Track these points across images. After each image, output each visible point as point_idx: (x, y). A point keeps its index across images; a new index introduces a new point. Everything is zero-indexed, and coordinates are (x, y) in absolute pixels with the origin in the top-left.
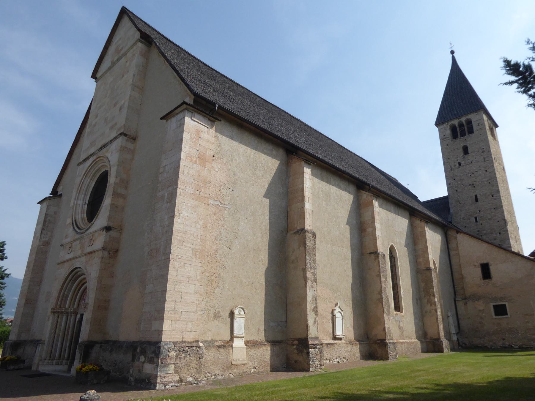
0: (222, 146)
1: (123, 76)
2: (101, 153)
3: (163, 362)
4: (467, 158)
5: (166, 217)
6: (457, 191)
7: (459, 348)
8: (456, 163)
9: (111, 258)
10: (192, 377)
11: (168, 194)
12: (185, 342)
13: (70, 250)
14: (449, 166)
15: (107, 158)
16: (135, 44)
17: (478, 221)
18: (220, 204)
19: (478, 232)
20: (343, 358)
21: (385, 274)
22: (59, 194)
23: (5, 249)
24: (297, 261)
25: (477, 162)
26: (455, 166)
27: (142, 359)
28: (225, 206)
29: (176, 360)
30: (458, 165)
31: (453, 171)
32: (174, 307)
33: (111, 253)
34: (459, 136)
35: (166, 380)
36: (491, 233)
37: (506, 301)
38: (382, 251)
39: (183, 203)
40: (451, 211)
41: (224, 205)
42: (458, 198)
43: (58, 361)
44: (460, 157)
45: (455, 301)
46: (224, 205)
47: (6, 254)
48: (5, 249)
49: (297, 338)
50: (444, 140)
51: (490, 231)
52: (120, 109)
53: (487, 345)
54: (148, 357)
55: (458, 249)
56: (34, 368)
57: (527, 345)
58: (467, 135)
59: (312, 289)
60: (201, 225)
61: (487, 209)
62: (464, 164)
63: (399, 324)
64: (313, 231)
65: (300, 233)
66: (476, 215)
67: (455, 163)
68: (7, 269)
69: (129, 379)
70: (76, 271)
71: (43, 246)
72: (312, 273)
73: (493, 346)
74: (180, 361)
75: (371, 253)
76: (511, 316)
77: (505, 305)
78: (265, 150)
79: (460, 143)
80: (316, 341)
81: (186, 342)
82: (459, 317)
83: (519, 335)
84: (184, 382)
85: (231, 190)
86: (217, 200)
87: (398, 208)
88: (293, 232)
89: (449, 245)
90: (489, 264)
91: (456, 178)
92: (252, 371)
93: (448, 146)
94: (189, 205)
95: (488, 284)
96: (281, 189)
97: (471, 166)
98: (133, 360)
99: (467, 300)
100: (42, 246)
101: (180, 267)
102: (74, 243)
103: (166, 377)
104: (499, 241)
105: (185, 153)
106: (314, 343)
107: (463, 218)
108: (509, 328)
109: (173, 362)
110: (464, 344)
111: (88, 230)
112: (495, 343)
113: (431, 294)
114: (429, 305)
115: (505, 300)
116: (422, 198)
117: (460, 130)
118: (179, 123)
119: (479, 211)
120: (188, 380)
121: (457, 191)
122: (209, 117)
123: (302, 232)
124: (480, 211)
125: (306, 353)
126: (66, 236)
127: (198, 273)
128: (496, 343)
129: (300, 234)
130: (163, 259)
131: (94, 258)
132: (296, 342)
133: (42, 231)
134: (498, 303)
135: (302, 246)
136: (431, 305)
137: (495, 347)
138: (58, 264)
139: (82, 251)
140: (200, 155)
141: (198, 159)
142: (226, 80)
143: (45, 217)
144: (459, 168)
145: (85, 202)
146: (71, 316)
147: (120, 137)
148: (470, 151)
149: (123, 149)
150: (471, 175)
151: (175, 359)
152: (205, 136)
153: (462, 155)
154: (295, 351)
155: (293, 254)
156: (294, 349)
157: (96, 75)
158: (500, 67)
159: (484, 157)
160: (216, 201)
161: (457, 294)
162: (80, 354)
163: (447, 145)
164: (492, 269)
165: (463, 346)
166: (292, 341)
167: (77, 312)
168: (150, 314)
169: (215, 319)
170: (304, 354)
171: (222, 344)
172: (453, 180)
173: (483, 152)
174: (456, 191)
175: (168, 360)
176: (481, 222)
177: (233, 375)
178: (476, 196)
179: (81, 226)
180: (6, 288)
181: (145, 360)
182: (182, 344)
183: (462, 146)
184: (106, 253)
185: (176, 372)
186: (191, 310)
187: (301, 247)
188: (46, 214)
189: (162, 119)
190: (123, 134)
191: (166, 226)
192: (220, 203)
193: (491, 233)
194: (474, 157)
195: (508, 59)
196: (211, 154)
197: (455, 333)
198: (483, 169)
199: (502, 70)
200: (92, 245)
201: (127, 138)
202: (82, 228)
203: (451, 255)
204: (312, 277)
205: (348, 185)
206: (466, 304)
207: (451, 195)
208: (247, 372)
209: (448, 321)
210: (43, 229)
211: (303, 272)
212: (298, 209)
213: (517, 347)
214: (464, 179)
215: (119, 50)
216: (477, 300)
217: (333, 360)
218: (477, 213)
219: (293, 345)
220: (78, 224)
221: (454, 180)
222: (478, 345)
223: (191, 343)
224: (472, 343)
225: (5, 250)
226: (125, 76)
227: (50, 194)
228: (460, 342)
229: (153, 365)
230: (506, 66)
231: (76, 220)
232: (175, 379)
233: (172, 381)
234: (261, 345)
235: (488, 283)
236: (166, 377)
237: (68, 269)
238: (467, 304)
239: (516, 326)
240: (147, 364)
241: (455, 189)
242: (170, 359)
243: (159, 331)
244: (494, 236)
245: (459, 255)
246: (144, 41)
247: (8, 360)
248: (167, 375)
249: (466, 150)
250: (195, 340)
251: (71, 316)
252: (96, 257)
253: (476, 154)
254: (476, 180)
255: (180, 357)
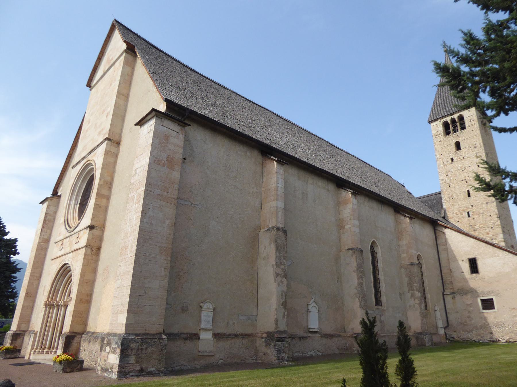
0: (194, 149)
1: (111, 85)
2: (89, 158)
3: (124, 353)
4: (460, 154)
5: (135, 217)
6: (449, 186)
7: (446, 341)
8: (448, 159)
9: (93, 254)
10: (154, 367)
11: (137, 196)
12: (148, 334)
13: (61, 248)
14: (441, 161)
15: (94, 161)
16: (122, 54)
17: (470, 215)
18: (190, 204)
19: (471, 227)
20: (317, 350)
21: (362, 269)
22: (58, 194)
23: (17, 246)
24: (268, 258)
25: (470, 157)
26: (448, 162)
27: (108, 349)
28: (196, 206)
29: (137, 351)
30: (450, 161)
31: (445, 167)
32: (137, 301)
33: (93, 250)
34: (459, 129)
35: (127, 370)
36: (484, 228)
37: (494, 296)
38: (360, 247)
39: (149, 204)
40: (444, 207)
41: (195, 205)
42: (451, 193)
43: (48, 350)
44: (453, 153)
45: (443, 295)
46: (195, 205)
47: (18, 250)
48: (17, 246)
49: (266, 331)
50: (437, 136)
51: (482, 225)
52: (107, 116)
53: (475, 339)
54: (112, 348)
55: (446, 244)
56: (27, 357)
57: (514, 339)
58: (459, 132)
59: (281, 284)
60: (168, 224)
61: (479, 204)
62: (456, 160)
63: (380, 318)
64: (284, 229)
65: (271, 231)
66: (468, 210)
67: (448, 158)
68: (18, 264)
69: (97, 368)
70: (65, 267)
71: (43, 243)
72: (282, 269)
73: (481, 340)
74: (141, 352)
75: (349, 249)
76: (498, 310)
77: (492, 299)
78: (239, 152)
79: (453, 138)
80: (283, 335)
81: (149, 334)
82: (448, 311)
83: (506, 329)
84: (145, 372)
85: (202, 191)
86: (187, 200)
87: (381, 205)
88: (265, 230)
89: (438, 240)
90: (477, 259)
91: (449, 174)
92: (220, 362)
93: (441, 143)
94: (156, 205)
95: (476, 278)
96: (255, 189)
97: (464, 162)
98: (101, 351)
99: (455, 295)
100: (41, 243)
101: (145, 263)
102: (65, 241)
103: (127, 367)
104: (492, 235)
105: (153, 157)
106: (282, 336)
107: (456, 213)
108: (497, 322)
109: (134, 353)
110: (452, 338)
111: (76, 228)
112: (482, 337)
113: (415, 288)
114: (413, 299)
115: (492, 294)
116: (417, 194)
117: (452, 126)
118: (149, 129)
119: (471, 206)
120: (149, 370)
121: (449, 186)
122: (178, 122)
123: (273, 230)
124: (472, 206)
125: (273, 346)
126: (59, 234)
127: (163, 269)
128: (483, 337)
129: (271, 232)
130: (130, 256)
131: (79, 254)
132: (265, 335)
133: (42, 229)
134: (486, 297)
135: (272, 243)
136: (415, 300)
137: (482, 341)
138: (52, 260)
139: (70, 248)
140: (168, 158)
141: (166, 162)
142: (213, 84)
143: (45, 216)
144: (452, 164)
145: (77, 203)
146: (62, 308)
147: (105, 142)
148: (462, 146)
149: (107, 153)
150: (463, 171)
151: (136, 350)
152: (174, 140)
153: (455, 150)
154: (264, 344)
155: (264, 250)
156: (263, 342)
157: (90, 83)
158: (432, 70)
159: (476, 153)
160: (187, 201)
161: (445, 288)
162: (62, 344)
163: (440, 141)
164: (480, 264)
165: (451, 340)
166: (261, 335)
167: (67, 305)
168: (117, 307)
169: (182, 313)
170: (271, 347)
171: (189, 336)
172: (446, 175)
173: (475, 147)
174: (448, 187)
175: (129, 351)
176: (474, 217)
177: (199, 365)
178: (468, 191)
179: (72, 225)
180: (17, 282)
181: (110, 350)
182: (144, 336)
183: (454, 142)
184: (89, 250)
185: (137, 362)
186: (155, 304)
187: (271, 244)
188: (46, 214)
189: (136, 125)
190: (108, 139)
191: (134, 225)
192: (191, 203)
193: (484, 228)
194: (467, 153)
195: (438, 62)
196: (180, 157)
197: (442, 326)
198: (475, 164)
199: (433, 73)
200: (78, 243)
201: (111, 142)
202: (73, 226)
203: (440, 249)
204: (282, 273)
205: (327, 184)
206: (454, 298)
207: (444, 190)
208: (214, 363)
209: (435, 314)
210: (43, 227)
211: (273, 268)
212: (271, 208)
213: (505, 341)
214: (457, 175)
215: (110, 60)
216: (465, 294)
217: (306, 353)
218: (469, 208)
219: (262, 338)
220: (70, 223)
221: (447, 175)
222: (466, 339)
223: (153, 335)
224: (460, 337)
225: (17, 247)
226: (113, 85)
227: (51, 195)
228: (447, 336)
229: (115, 356)
230: (436, 69)
231: (68, 219)
232: (136, 369)
233: (132, 371)
234: (229, 338)
235: (476, 277)
236: (127, 367)
237: (59, 265)
238: (455, 298)
239: (503, 320)
240: (111, 354)
241: (448, 184)
242: (132, 350)
243: (123, 323)
244: (487, 230)
245: (447, 250)
246: (130, 52)
247: (4, 350)
248: (128, 365)
249: (458, 146)
250: (158, 332)
251: (61, 308)
252: (80, 254)
253: (469, 149)
254: (468, 175)
255: (142, 349)
